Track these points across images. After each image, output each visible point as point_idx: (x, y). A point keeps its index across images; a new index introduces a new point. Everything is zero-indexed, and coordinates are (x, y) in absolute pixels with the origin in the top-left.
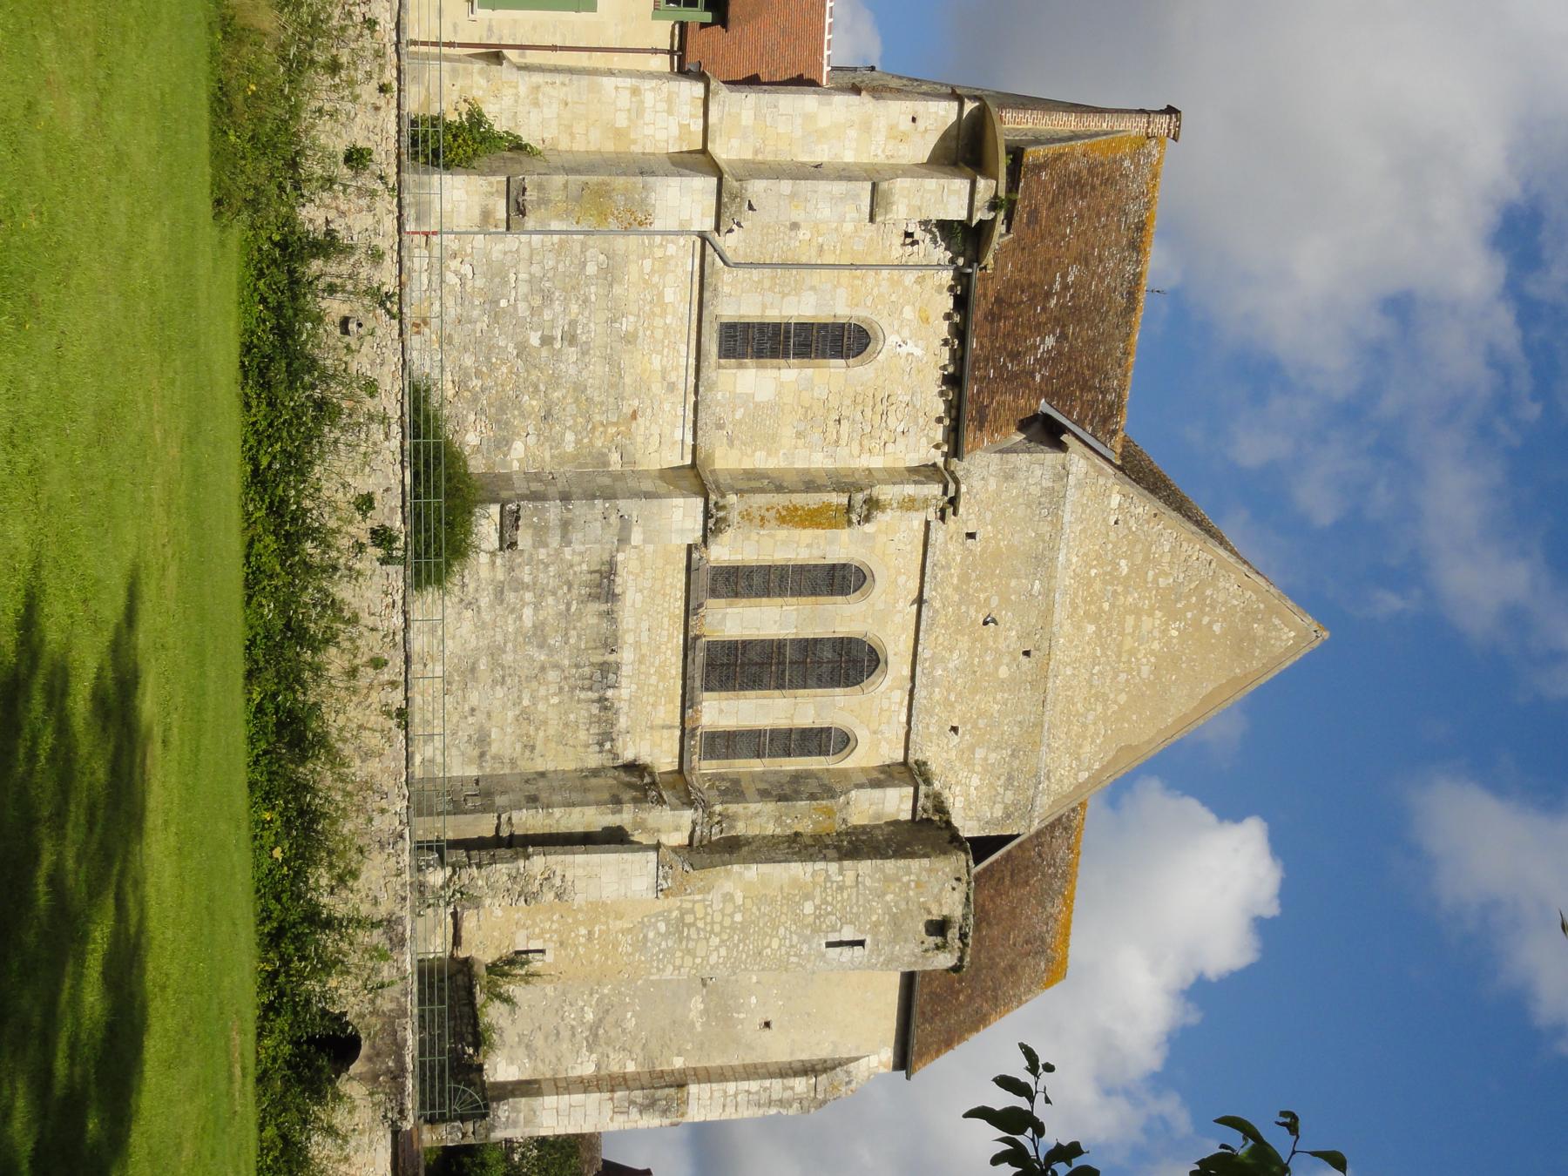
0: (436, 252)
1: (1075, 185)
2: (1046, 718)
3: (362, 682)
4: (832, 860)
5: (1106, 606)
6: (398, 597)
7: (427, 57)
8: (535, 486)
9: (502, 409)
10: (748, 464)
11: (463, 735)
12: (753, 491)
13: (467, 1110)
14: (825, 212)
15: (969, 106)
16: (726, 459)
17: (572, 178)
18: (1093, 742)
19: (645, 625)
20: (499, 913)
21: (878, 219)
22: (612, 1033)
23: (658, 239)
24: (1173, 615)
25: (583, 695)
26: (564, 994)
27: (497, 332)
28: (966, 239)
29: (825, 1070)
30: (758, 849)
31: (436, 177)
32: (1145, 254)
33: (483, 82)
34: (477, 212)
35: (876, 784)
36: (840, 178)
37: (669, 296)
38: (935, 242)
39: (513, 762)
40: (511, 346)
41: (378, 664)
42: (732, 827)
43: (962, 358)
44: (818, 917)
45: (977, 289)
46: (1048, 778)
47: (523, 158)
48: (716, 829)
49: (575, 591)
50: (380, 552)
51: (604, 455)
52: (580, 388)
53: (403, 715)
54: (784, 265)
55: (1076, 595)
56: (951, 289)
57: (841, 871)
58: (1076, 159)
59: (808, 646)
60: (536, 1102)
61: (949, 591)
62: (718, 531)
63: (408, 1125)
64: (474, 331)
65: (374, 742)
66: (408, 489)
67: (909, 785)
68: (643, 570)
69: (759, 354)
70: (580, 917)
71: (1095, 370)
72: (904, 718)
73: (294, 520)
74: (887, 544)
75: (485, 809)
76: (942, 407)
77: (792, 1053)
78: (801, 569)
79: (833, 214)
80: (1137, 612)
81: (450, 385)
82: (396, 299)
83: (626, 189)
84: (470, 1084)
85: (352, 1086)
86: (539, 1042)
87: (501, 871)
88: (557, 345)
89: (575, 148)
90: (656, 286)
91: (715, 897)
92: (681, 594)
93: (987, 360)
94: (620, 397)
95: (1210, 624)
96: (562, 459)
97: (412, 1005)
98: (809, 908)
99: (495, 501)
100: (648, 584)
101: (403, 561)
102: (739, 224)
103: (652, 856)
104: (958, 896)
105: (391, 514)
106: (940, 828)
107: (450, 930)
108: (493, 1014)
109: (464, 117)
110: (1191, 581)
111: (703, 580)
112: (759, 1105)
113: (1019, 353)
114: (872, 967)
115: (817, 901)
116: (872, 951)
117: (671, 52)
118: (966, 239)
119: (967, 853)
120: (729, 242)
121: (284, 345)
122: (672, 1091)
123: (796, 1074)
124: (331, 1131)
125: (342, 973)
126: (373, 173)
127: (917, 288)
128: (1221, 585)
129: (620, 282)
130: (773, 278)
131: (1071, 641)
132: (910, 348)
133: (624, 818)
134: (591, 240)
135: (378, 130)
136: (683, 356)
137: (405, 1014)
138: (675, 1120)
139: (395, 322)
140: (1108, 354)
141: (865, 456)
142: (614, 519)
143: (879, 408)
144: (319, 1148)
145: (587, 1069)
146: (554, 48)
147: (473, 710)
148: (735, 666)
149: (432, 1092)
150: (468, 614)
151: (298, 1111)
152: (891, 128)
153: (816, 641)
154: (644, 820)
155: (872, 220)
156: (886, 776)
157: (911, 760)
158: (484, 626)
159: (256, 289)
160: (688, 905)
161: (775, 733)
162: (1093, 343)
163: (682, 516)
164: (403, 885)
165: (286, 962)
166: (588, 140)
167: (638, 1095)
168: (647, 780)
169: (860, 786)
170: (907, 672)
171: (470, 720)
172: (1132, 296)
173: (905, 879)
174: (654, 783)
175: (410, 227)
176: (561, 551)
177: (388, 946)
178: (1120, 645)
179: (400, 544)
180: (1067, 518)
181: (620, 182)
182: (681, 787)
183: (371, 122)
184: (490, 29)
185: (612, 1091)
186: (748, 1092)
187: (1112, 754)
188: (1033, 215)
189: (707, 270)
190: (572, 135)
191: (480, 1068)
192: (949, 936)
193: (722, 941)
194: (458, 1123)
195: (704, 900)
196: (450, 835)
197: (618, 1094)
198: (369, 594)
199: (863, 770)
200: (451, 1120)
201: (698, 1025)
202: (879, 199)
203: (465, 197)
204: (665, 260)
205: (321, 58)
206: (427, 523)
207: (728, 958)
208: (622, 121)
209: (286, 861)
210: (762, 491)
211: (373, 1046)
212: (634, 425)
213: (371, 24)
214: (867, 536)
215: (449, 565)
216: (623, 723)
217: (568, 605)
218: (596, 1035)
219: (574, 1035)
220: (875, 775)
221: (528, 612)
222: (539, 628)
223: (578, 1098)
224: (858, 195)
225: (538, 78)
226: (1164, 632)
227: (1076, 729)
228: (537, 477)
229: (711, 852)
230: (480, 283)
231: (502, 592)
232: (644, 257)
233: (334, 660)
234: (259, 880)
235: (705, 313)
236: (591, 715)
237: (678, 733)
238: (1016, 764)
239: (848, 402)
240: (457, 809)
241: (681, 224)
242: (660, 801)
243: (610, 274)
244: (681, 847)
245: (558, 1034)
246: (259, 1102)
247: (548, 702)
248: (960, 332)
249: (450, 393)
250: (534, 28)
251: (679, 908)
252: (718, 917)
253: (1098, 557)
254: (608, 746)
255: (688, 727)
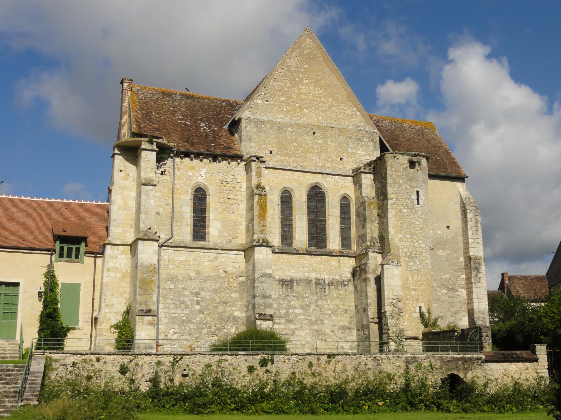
0: (165, 342)
1: (147, 115)
2: (337, 126)
3: (318, 370)
4: (387, 202)
5: (297, 105)
6: (286, 357)
7: (95, 343)
8: (250, 308)
9: (223, 319)
10: (244, 232)
11: (342, 335)
12: (253, 229)
13: (478, 335)
14: (152, 202)
15: (116, 151)
16: (242, 239)
17: (137, 293)
18: (346, 110)
19: (302, 269)
20: (406, 323)
21: (155, 183)
22: (451, 283)
23: (162, 262)
24: (301, 81)
25: (327, 292)
26: (436, 300)
27: (194, 321)
28: (163, 153)
29: (465, 207)
30: (383, 229)
31: (136, 342)
32: (174, 92)
33: (104, 324)
34: (149, 327)
35: (360, 187)
36: (140, 197)
37: (182, 258)
38: (165, 164)
39: (351, 317)
40: (199, 316)
41: (311, 365)
42: (375, 239)
43: (207, 155)
44: (408, 207)
45: (182, 149)
46: (359, 126)
47: (132, 310)
48: (376, 244)
49: (289, 294)
50: (269, 364)
51: (240, 282)
52: (215, 291)
53: (329, 356)
54: (172, 217)
55: (293, 116)
56: (182, 158)
57: (392, 199)
58: (138, 115)
59: (311, 211)
60: (476, 310)
61: (291, 160)
62: (267, 242)
63: (483, 357)
64: (194, 329)
65: (340, 367)
66: (246, 353)
67: (360, 176)
68: (282, 269)
69: (204, 227)
70: (407, 293)
71: (213, 109)
72: (337, 177)
73: (256, 396)
74: (273, 183)
75: (368, 327)
76: (224, 162)
77: (458, 218)
78: (282, 213)
79: (154, 199)
80: (299, 94)
81: (214, 338)
82: (175, 357)
83: (142, 273)
84: (468, 334)
85: (469, 377)
86: (454, 309)
87: (390, 322)
88: (200, 299)
89: (128, 291)
90: (179, 263)
91: (400, 244)
92: (291, 256)
93: (208, 146)
94: (219, 277)
95: (304, 68)
96: (241, 298)
97: (438, 355)
98: (405, 211)
99: (255, 322)
100: (287, 268)
101: (273, 355)
102: (156, 233)
103: (385, 267)
104: (401, 157)
105: (255, 360)
106: (376, 164)
107: (412, 340)
108: (443, 325)
109: (117, 331)
110: (289, 75)
111: (286, 248)
112: (477, 230)
113: (206, 135)
114: (427, 189)
115: (402, 208)
116: (421, 188)
117: (96, 257)
118: (163, 153)
119: (385, 154)
120: (163, 238)
121: (190, 398)
122: (472, 261)
123: (466, 217)
124: (486, 385)
125: (426, 380)
126: (128, 364)
127: (181, 170)
128: (290, 65)
129: (177, 276)
130: (177, 221)
131: (310, 118)
132: (203, 173)
133: (372, 277)
134: (162, 286)
135: (113, 362)
136: (204, 254)
137: (442, 357)
138: (483, 261)
139: (184, 357)
140: (208, 105)
141: (242, 189)
142: (262, 279)
143: (224, 184)
144: (492, 390)
145: (464, 292)
146: (93, 299)
147: (332, 331)
148: (317, 237)
149: (471, 348)
150: (297, 332)
151: (478, 397)
152: (123, 179)
153: (308, 208)
154: (373, 270)
155: (155, 185)
156: (358, 183)
157: (352, 175)
158: (301, 327)
159: (169, 408)
160: (403, 254)
161: (342, 223)
162: (204, 110)
163: (262, 254)
164: (393, 357)
165: (421, 401)
166: (126, 287)
167: (473, 274)
168: (358, 269)
169: (361, 193)
170: (320, 176)
171: (336, 332)
172: (188, 97)
173: (394, 176)
174: (359, 267)
175: (154, 351)
176: (274, 298)
177: (416, 363)
178: (312, 100)
179: (266, 357)
180: (265, 118)
181: (139, 275)
182: (361, 257)
183: (110, 365)
184: (86, 322)
185: (472, 283)
186: (472, 234)
187: (350, 103)
188: (156, 129)
189: (173, 245)
190: (124, 293)
191: (462, 330)
192: (415, 160)
193: (417, 242)
194: (483, 338)
195: (402, 248)
196: (378, 340)
197: (473, 281)
198: (285, 368)
199: (355, 191)
200: (481, 341)
201: (448, 252)
202: (148, 183)
203: (144, 331)
204: (169, 260)
205: (84, 382)
206: (262, 346)
207: (423, 240)
208: (119, 275)
209: (384, 400)
210: (253, 226)
211: (454, 369)
212: (229, 272)
213: (74, 364)
214: (271, 189)
215: (277, 339)
216: (337, 277)
217: (294, 296)
218: (452, 289)
219: (451, 297)
220: (357, 187)
221: (297, 311)
222: (302, 307)
223: (474, 296)
224: (146, 190)
225: (103, 305)
226: (307, 85)
227: (341, 116)
228: (247, 307)
229: (384, 246)
230: (176, 327)
231: (289, 320)
232: (168, 267)
233: (309, 381)
234: (391, 411)
235: (189, 246)
236: (335, 289)
237: (341, 258)
238: (354, 138)
239: (222, 196)
240: (368, 338)
241: (155, 254)
242: (366, 264)
243: (174, 280)
244: (382, 257)
245: (451, 303)
246: (474, 412)
247: (330, 304)
248: (197, 155)
249: (216, 338)
250: (86, 306)
251: (405, 257)
252: (408, 243)
253: (279, 108)
254: (346, 283)
255: (339, 254)
